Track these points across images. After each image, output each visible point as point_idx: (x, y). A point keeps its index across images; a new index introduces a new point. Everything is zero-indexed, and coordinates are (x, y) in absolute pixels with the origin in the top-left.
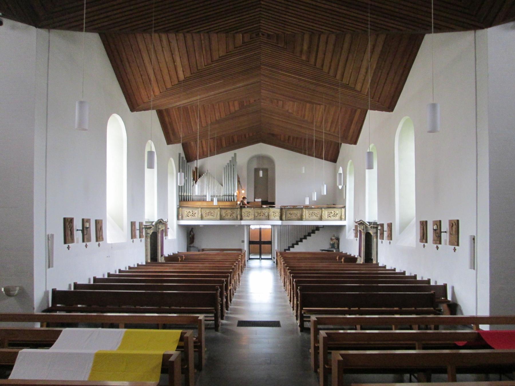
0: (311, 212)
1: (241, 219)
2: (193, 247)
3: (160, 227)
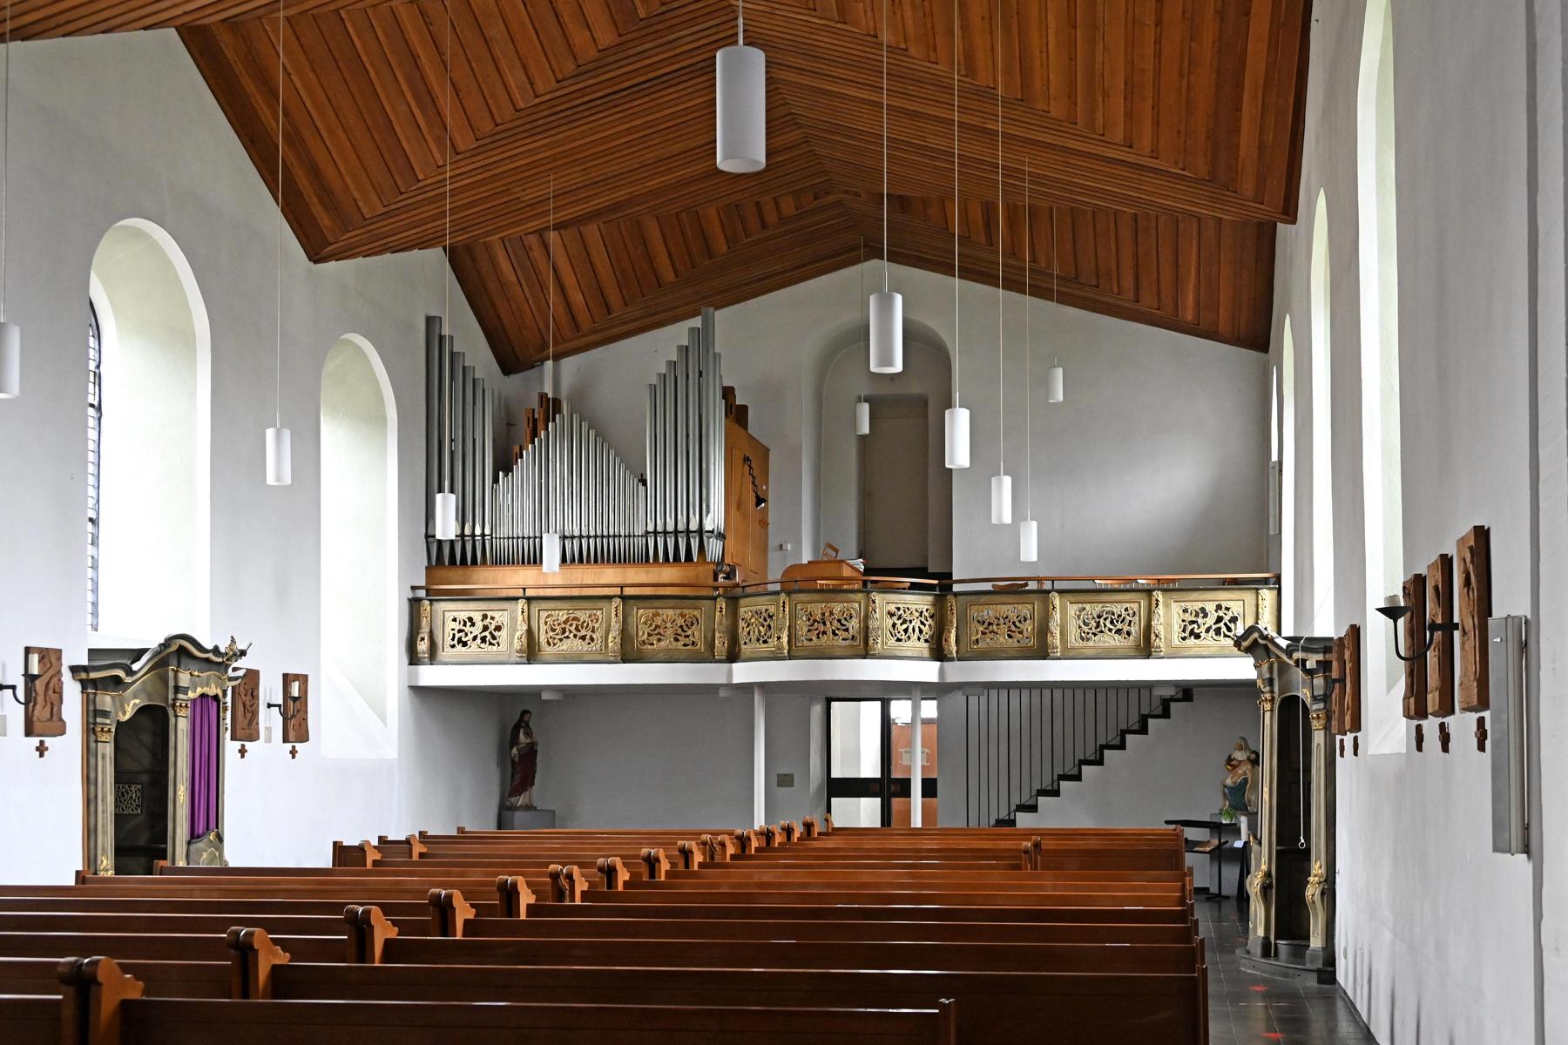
0: (1093, 609)
1: (733, 657)
2: (529, 807)
3: (184, 679)
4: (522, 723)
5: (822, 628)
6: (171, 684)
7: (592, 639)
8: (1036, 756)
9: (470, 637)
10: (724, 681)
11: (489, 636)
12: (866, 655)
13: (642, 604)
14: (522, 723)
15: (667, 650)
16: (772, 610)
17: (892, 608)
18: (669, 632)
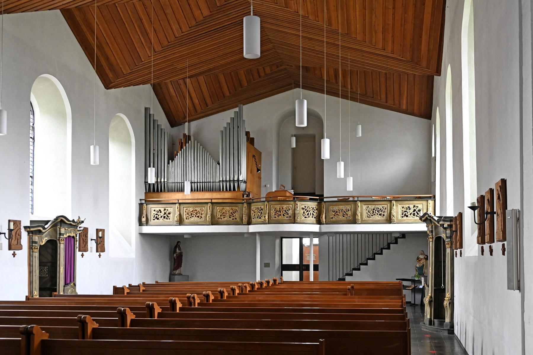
0: (372, 207)
1: (249, 223)
2: (180, 274)
4: (177, 246)
5: (279, 213)
6: (58, 232)
7: (201, 217)
8: (352, 257)
9: (160, 216)
10: (246, 231)
11: (166, 216)
12: (294, 222)
13: (218, 205)
14: (177, 246)
15: (227, 221)
16: (262, 207)
17: (303, 206)
18: (228, 215)
